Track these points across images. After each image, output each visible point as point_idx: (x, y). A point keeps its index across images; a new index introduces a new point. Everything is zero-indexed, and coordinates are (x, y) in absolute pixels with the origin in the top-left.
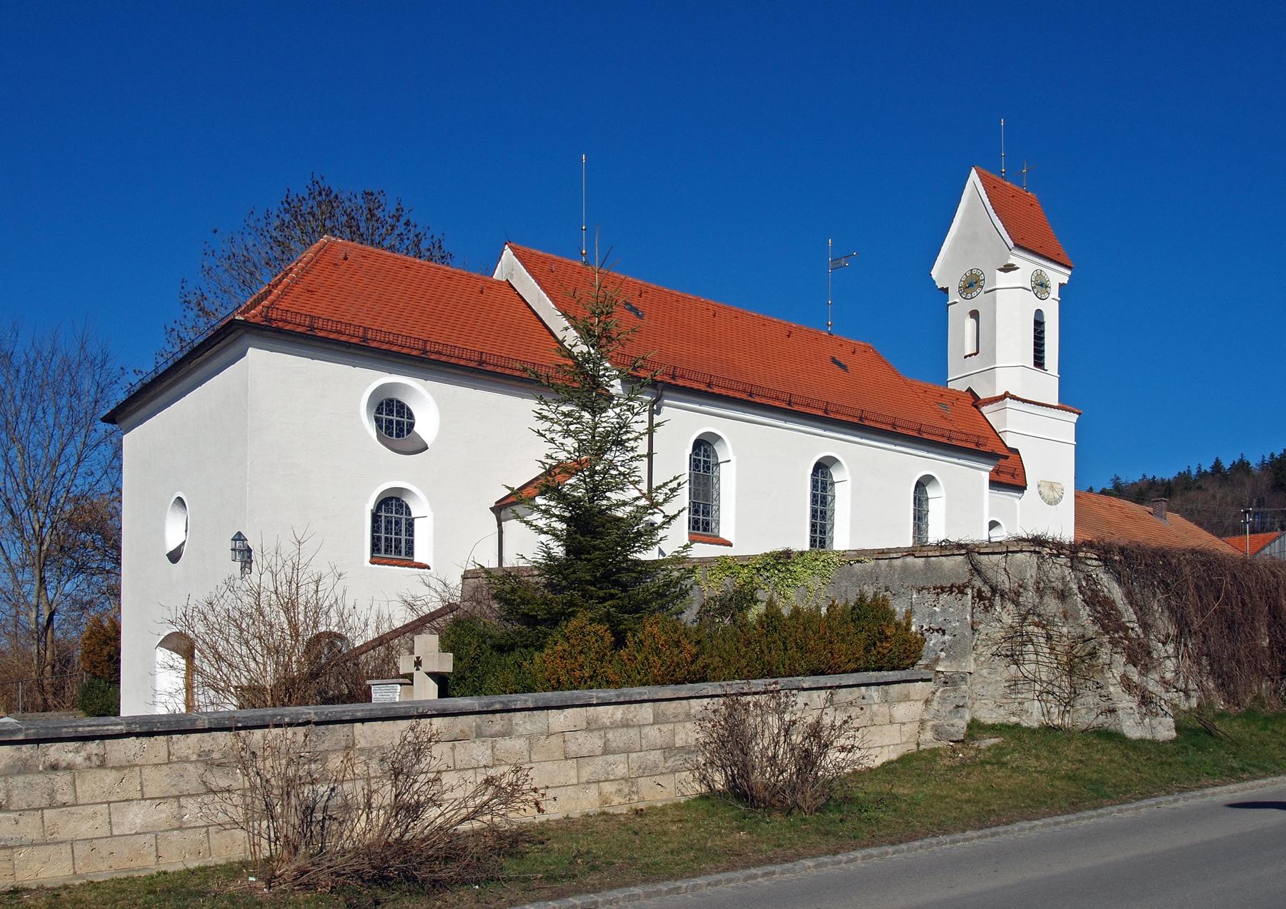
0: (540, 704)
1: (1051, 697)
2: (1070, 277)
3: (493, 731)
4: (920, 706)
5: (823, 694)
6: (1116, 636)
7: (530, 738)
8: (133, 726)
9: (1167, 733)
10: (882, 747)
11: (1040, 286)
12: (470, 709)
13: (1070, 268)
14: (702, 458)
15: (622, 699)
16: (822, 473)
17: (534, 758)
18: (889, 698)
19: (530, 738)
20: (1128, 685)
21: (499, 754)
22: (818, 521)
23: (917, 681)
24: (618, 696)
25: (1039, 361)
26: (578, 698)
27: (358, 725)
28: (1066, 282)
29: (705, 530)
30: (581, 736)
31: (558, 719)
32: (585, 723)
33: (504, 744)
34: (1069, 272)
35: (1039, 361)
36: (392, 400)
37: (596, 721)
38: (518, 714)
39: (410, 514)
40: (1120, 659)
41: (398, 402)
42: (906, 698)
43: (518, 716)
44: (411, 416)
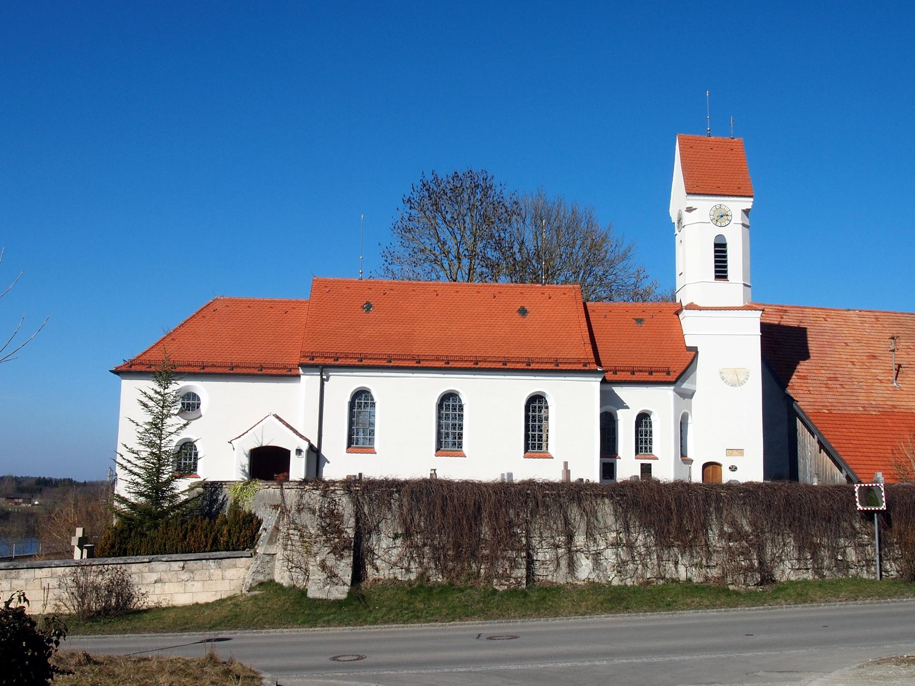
0: (29, 566)
1: (298, 570)
2: (753, 202)
3: (11, 577)
4: (243, 570)
5: (181, 564)
6: (331, 536)
7: (27, 580)
8: (786, 523)
9: (340, 595)
10: (216, 591)
11: (721, 217)
12: (225, 556)
13: (752, 197)
14: (363, 401)
15: (66, 565)
16: (453, 399)
17: (27, 588)
18: (222, 566)
19: (27, 580)
20: (323, 566)
21: (13, 586)
22: (537, 414)
23: (242, 557)
24: (64, 564)
25: (721, 272)
26: (45, 564)
27: (37, 570)
28: (750, 207)
29: (357, 444)
30: (48, 580)
31: (38, 573)
32: (50, 575)
33: (15, 582)
34: (752, 199)
35: (721, 272)
36: (190, 393)
37: (56, 574)
38: (22, 570)
39: (196, 450)
40: (327, 550)
41: (193, 393)
42: (235, 566)
43: (22, 571)
44: (199, 399)
